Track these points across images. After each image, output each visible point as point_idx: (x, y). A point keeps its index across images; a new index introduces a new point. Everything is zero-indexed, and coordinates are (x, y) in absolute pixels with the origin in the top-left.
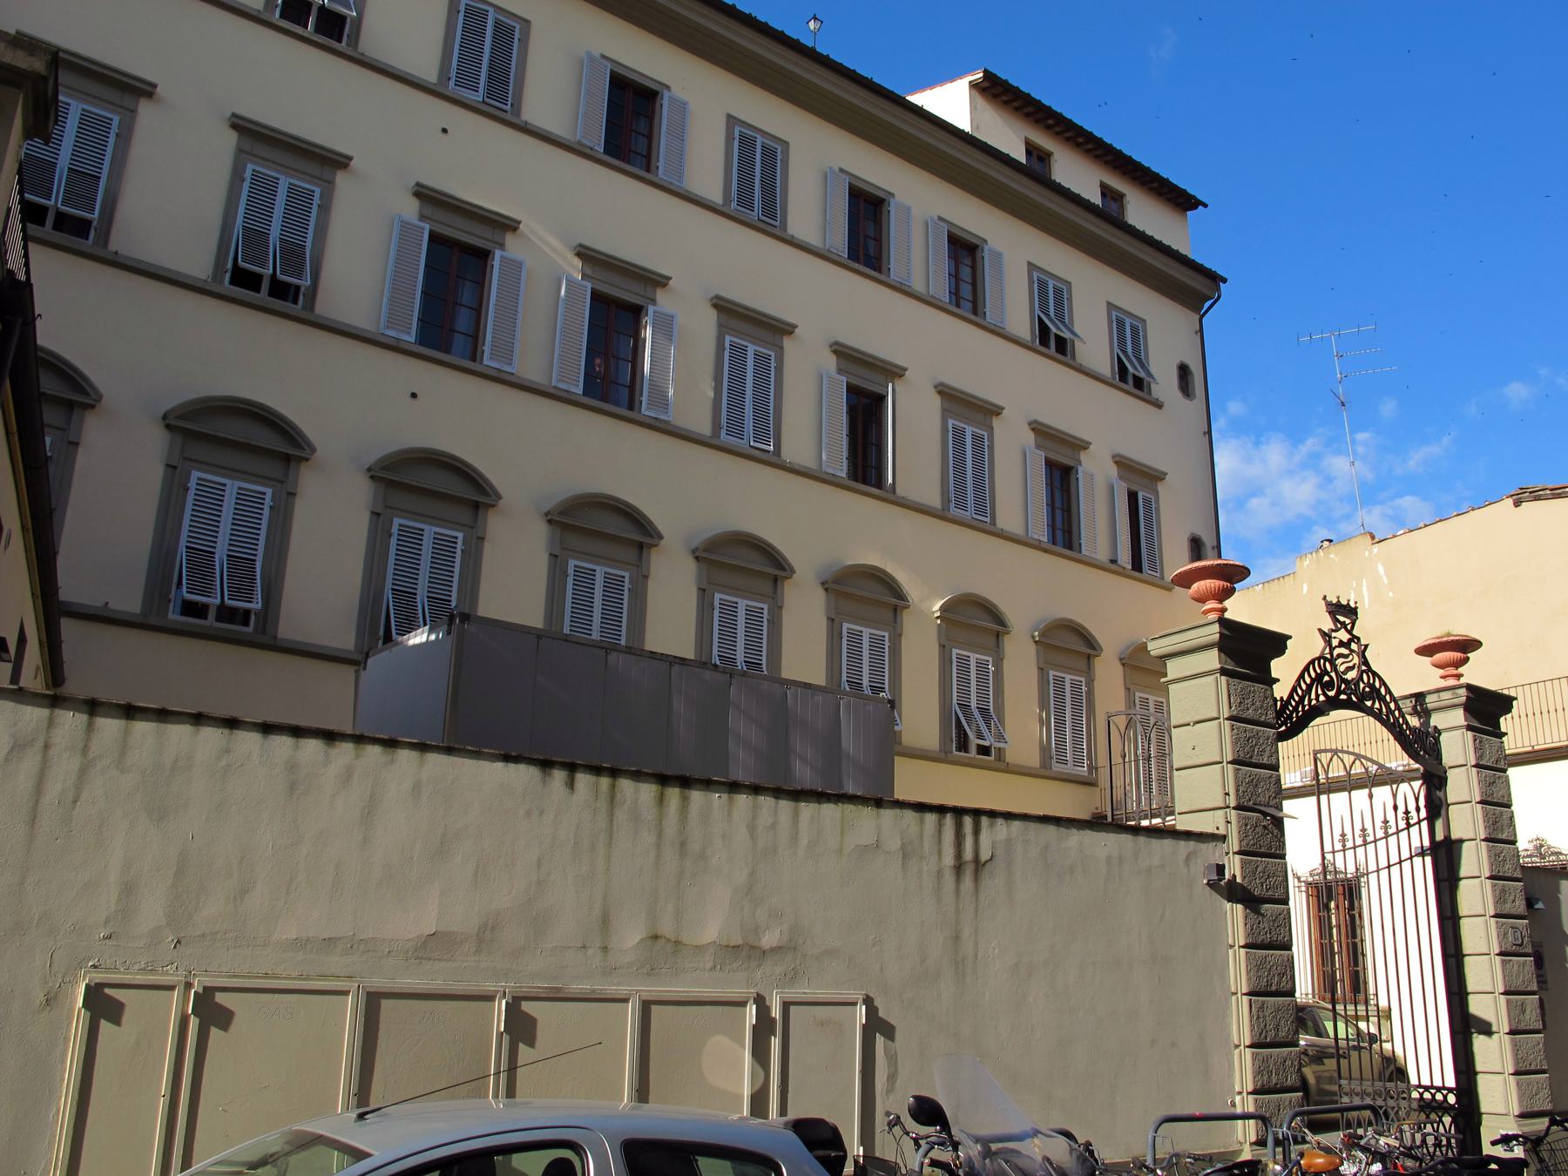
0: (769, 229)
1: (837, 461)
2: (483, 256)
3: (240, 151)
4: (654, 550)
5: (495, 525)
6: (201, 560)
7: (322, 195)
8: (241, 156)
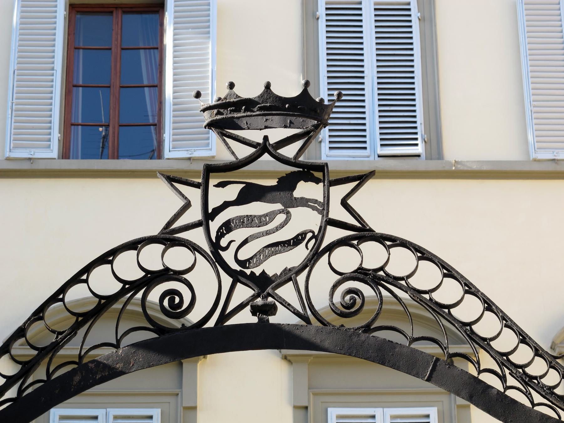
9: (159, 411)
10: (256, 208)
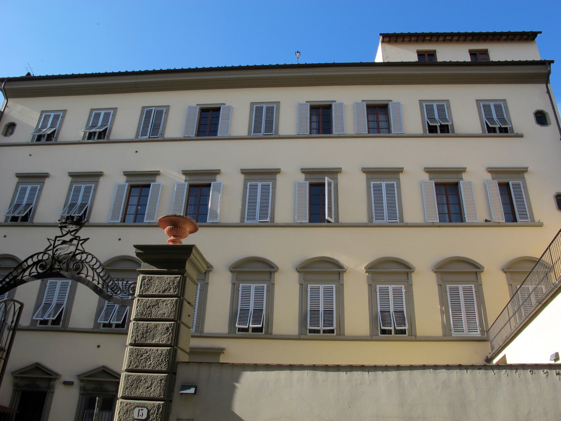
0: (268, 136)
1: (499, 215)
2: (456, 185)
3: (245, 180)
4: (413, 274)
5: (485, 278)
8: (368, 180)
9: (453, 335)
10: (64, 246)
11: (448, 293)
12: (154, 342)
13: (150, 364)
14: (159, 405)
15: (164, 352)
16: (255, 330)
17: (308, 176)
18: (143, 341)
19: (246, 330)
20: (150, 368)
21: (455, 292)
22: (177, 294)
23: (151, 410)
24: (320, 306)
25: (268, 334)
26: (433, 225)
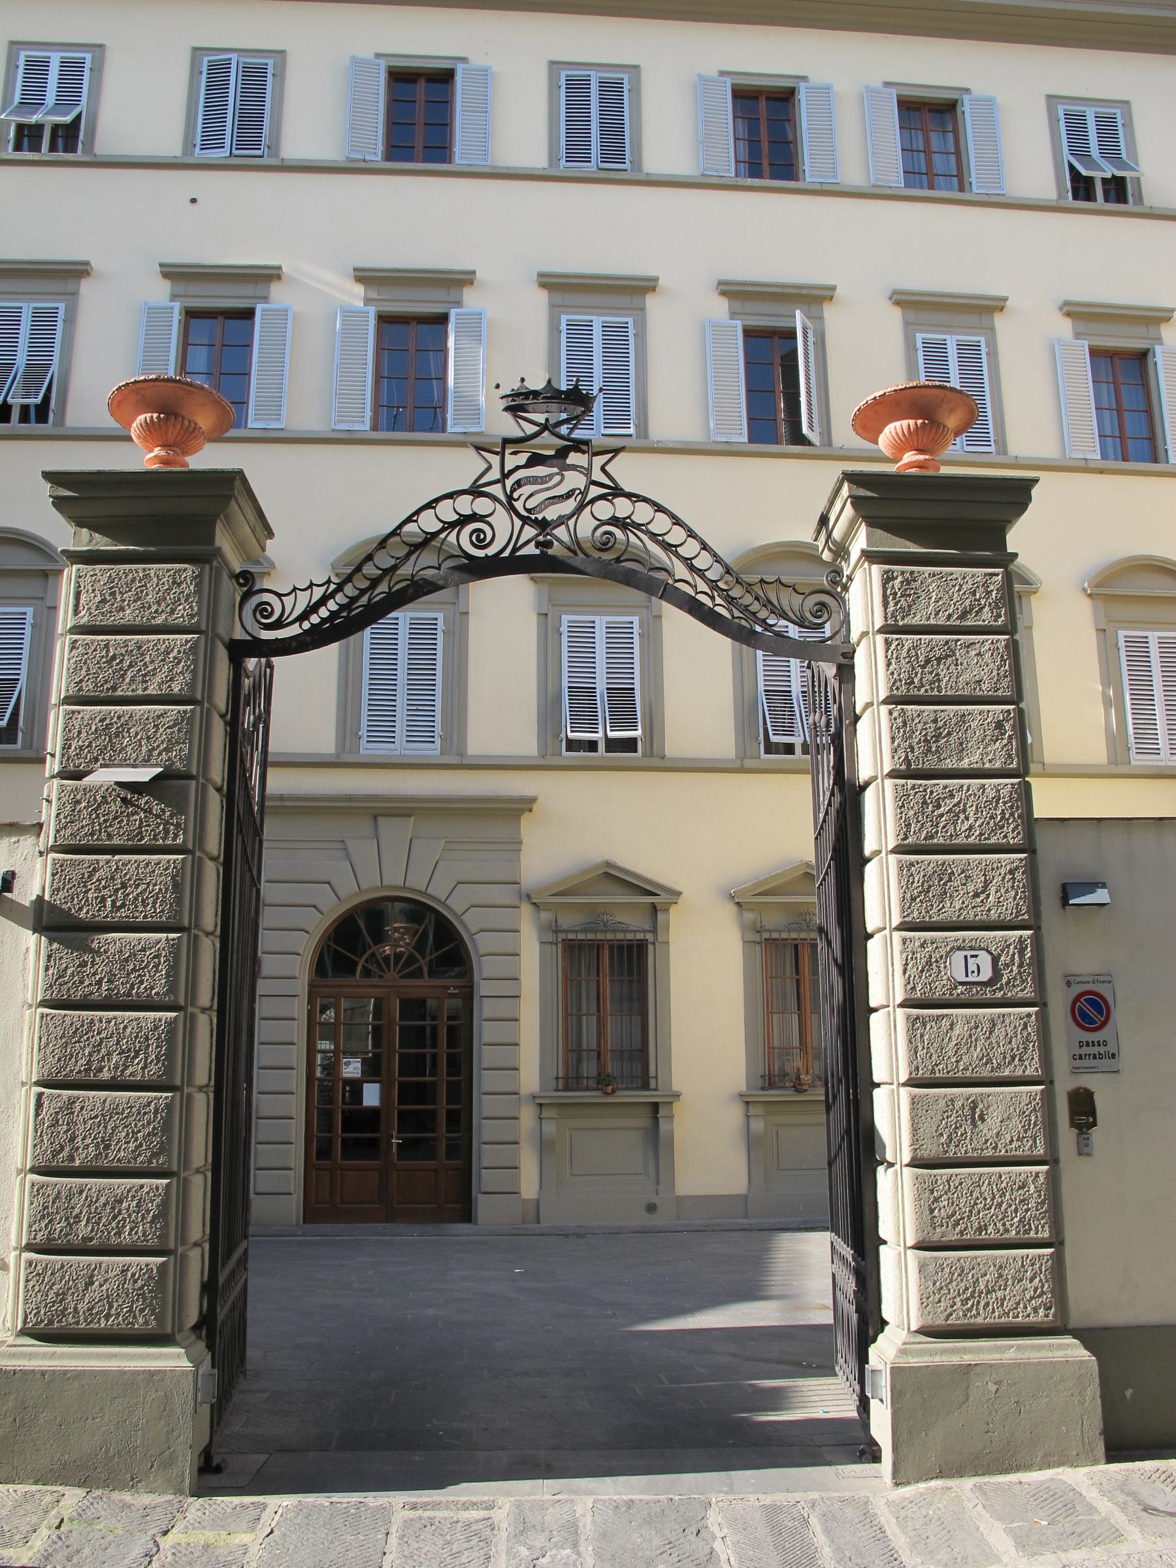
0: (613, 175)
2: (1142, 356)
3: (552, 306)
4: (1033, 597)
6: (583, 695)
7: (987, 346)
9: (1133, 763)
10: (540, 471)
11: (1123, 654)
12: (965, 764)
13: (971, 828)
14: (1021, 940)
15: (1005, 792)
16: (613, 745)
17: (738, 306)
18: (931, 763)
19: (592, 746)
20: (971, 840)
21: (1138, 650)
22: (1004, 625)
23: (999, 956)
24: (793, 679)
25: (652, 755)
26: (1085, 468)
